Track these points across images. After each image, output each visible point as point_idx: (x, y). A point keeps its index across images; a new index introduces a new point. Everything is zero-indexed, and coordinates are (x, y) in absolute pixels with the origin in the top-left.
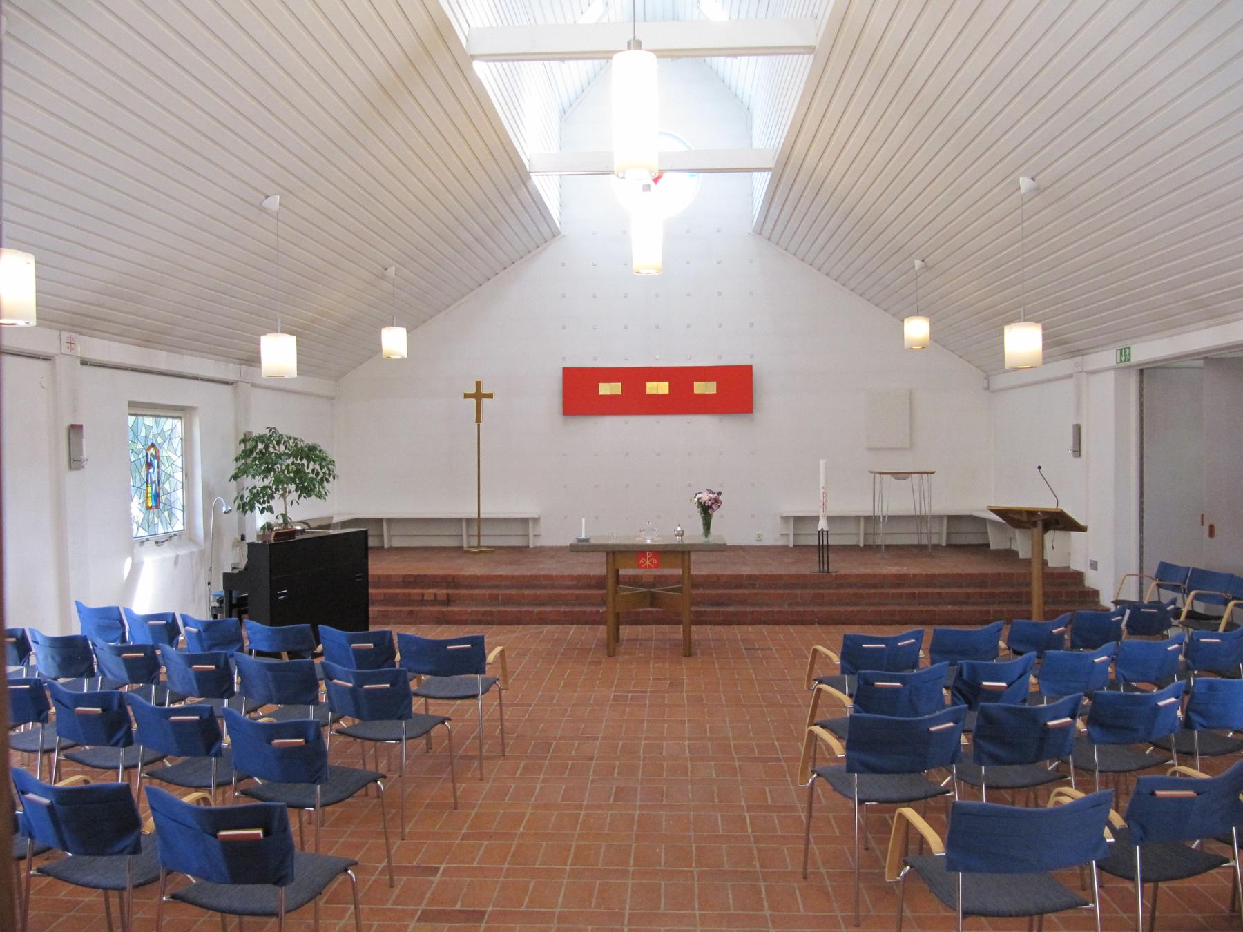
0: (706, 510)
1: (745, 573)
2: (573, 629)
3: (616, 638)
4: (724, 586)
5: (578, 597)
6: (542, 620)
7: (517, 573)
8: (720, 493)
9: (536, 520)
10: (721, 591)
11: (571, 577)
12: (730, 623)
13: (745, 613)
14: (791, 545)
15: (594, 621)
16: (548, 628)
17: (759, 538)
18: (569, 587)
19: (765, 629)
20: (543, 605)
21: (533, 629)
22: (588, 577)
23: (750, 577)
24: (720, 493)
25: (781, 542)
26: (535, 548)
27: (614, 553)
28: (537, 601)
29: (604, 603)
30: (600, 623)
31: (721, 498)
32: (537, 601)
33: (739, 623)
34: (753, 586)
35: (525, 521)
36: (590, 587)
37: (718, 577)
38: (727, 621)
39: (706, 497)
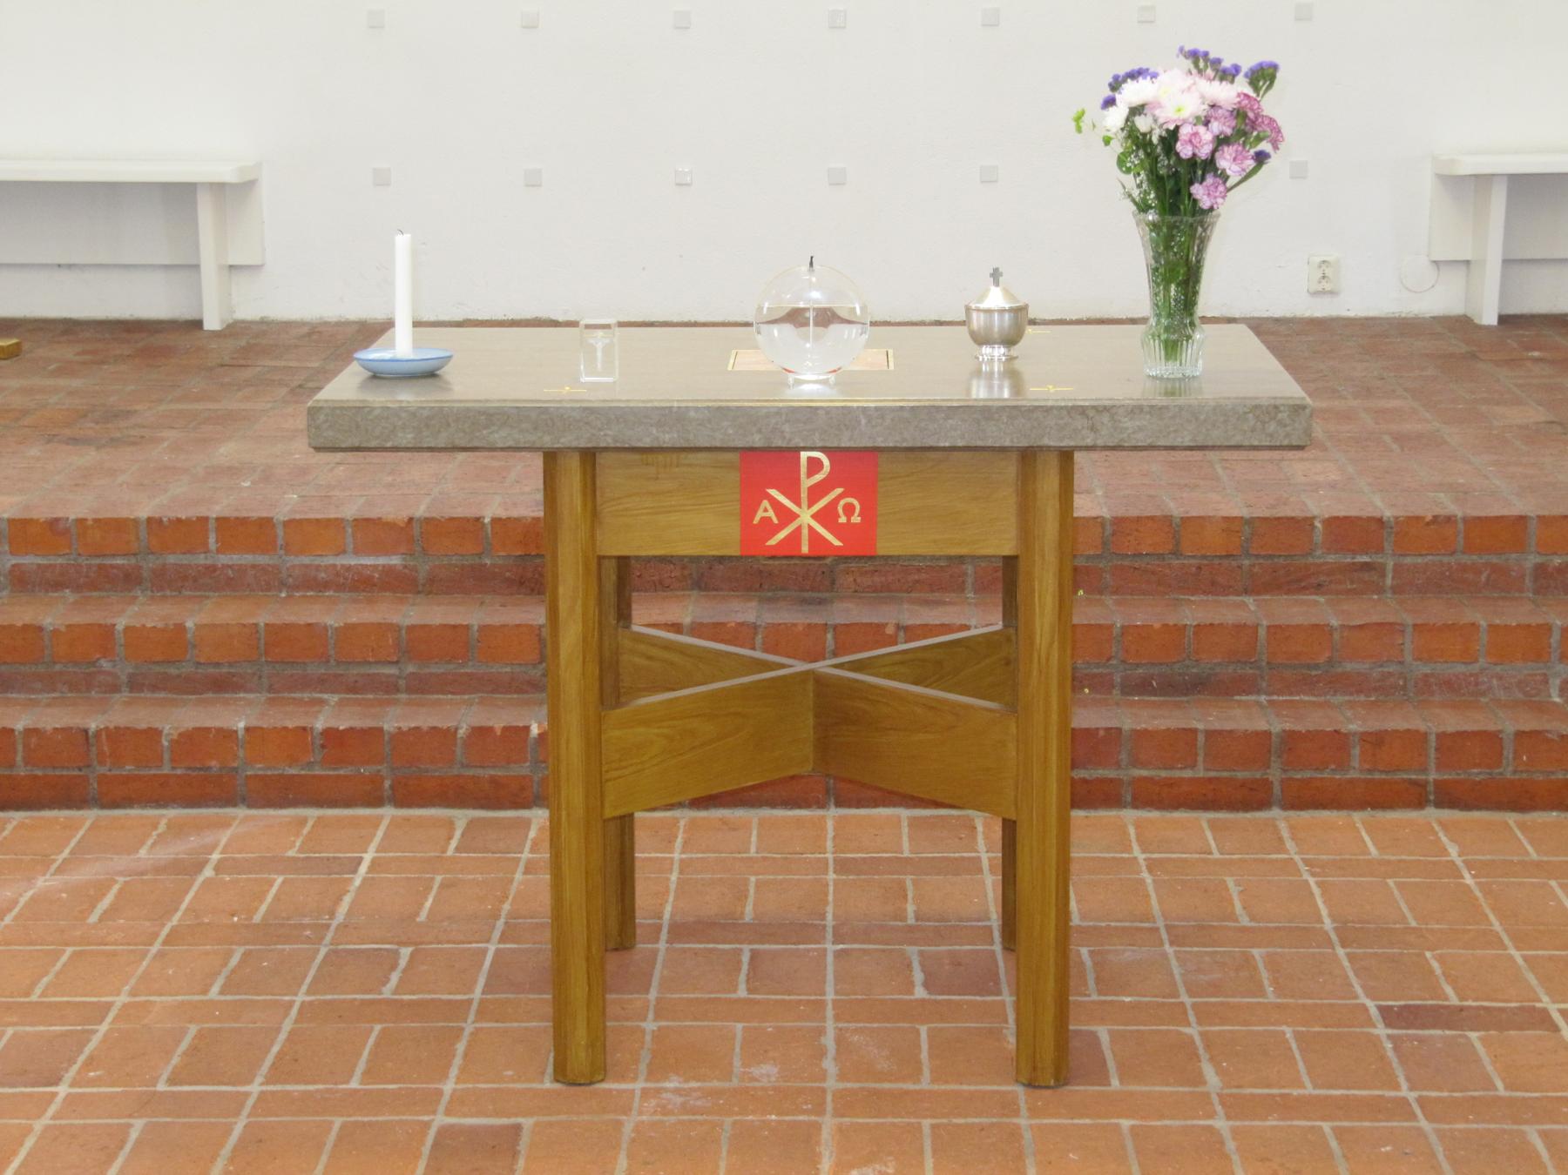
0: (1173, 184)
1: (1319, 507)
2: (376, 839)
3: (606, 913)
4: (1209, 578)
5: (418, 643)
6: (205, 779)
7: (79, 506)
8: (1263, 76)
9: (233, 195)
10: (1193, 612)
11: (372, 531)
12: (1253, 798)
13: (1338, 742)
14: (1490, 318)
15: (486, 780)
16: (236, 830)
17: (1326, 281)
18: (362, 585)
19: (1448, 835)
20: (222, 685)
21: (153, 837)
22: (470, 527)
23: (1347, 531)
24: (1263, 76)
25: (1437, 299)
26: (235, 329)
27: (589, 456)
28: (168, 668)
29: (535, 683)
30: (519, 796)
31: (1271, 104)
32: (168, 668)
33: (1303, 798)
34: (1364, 579)
35: (178, 197)
36: (473, 581)
37: (1176, 530)
38: (1238, 784)
39: (1178, 99)
